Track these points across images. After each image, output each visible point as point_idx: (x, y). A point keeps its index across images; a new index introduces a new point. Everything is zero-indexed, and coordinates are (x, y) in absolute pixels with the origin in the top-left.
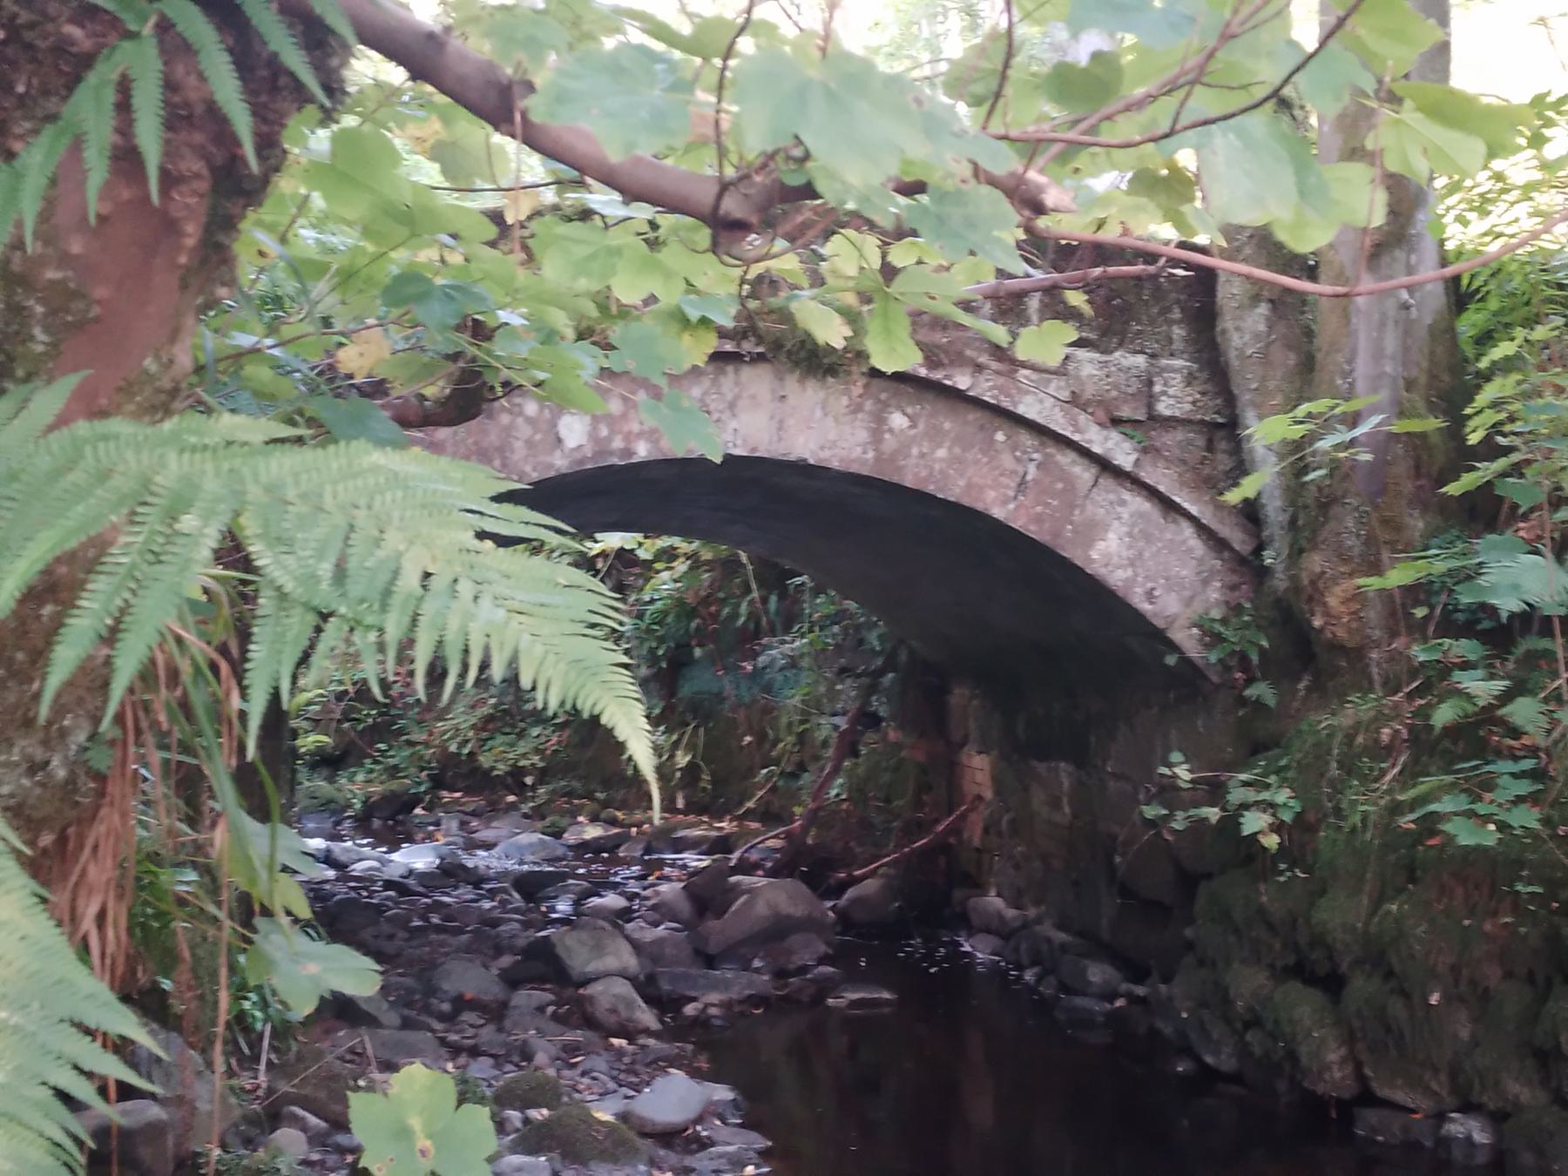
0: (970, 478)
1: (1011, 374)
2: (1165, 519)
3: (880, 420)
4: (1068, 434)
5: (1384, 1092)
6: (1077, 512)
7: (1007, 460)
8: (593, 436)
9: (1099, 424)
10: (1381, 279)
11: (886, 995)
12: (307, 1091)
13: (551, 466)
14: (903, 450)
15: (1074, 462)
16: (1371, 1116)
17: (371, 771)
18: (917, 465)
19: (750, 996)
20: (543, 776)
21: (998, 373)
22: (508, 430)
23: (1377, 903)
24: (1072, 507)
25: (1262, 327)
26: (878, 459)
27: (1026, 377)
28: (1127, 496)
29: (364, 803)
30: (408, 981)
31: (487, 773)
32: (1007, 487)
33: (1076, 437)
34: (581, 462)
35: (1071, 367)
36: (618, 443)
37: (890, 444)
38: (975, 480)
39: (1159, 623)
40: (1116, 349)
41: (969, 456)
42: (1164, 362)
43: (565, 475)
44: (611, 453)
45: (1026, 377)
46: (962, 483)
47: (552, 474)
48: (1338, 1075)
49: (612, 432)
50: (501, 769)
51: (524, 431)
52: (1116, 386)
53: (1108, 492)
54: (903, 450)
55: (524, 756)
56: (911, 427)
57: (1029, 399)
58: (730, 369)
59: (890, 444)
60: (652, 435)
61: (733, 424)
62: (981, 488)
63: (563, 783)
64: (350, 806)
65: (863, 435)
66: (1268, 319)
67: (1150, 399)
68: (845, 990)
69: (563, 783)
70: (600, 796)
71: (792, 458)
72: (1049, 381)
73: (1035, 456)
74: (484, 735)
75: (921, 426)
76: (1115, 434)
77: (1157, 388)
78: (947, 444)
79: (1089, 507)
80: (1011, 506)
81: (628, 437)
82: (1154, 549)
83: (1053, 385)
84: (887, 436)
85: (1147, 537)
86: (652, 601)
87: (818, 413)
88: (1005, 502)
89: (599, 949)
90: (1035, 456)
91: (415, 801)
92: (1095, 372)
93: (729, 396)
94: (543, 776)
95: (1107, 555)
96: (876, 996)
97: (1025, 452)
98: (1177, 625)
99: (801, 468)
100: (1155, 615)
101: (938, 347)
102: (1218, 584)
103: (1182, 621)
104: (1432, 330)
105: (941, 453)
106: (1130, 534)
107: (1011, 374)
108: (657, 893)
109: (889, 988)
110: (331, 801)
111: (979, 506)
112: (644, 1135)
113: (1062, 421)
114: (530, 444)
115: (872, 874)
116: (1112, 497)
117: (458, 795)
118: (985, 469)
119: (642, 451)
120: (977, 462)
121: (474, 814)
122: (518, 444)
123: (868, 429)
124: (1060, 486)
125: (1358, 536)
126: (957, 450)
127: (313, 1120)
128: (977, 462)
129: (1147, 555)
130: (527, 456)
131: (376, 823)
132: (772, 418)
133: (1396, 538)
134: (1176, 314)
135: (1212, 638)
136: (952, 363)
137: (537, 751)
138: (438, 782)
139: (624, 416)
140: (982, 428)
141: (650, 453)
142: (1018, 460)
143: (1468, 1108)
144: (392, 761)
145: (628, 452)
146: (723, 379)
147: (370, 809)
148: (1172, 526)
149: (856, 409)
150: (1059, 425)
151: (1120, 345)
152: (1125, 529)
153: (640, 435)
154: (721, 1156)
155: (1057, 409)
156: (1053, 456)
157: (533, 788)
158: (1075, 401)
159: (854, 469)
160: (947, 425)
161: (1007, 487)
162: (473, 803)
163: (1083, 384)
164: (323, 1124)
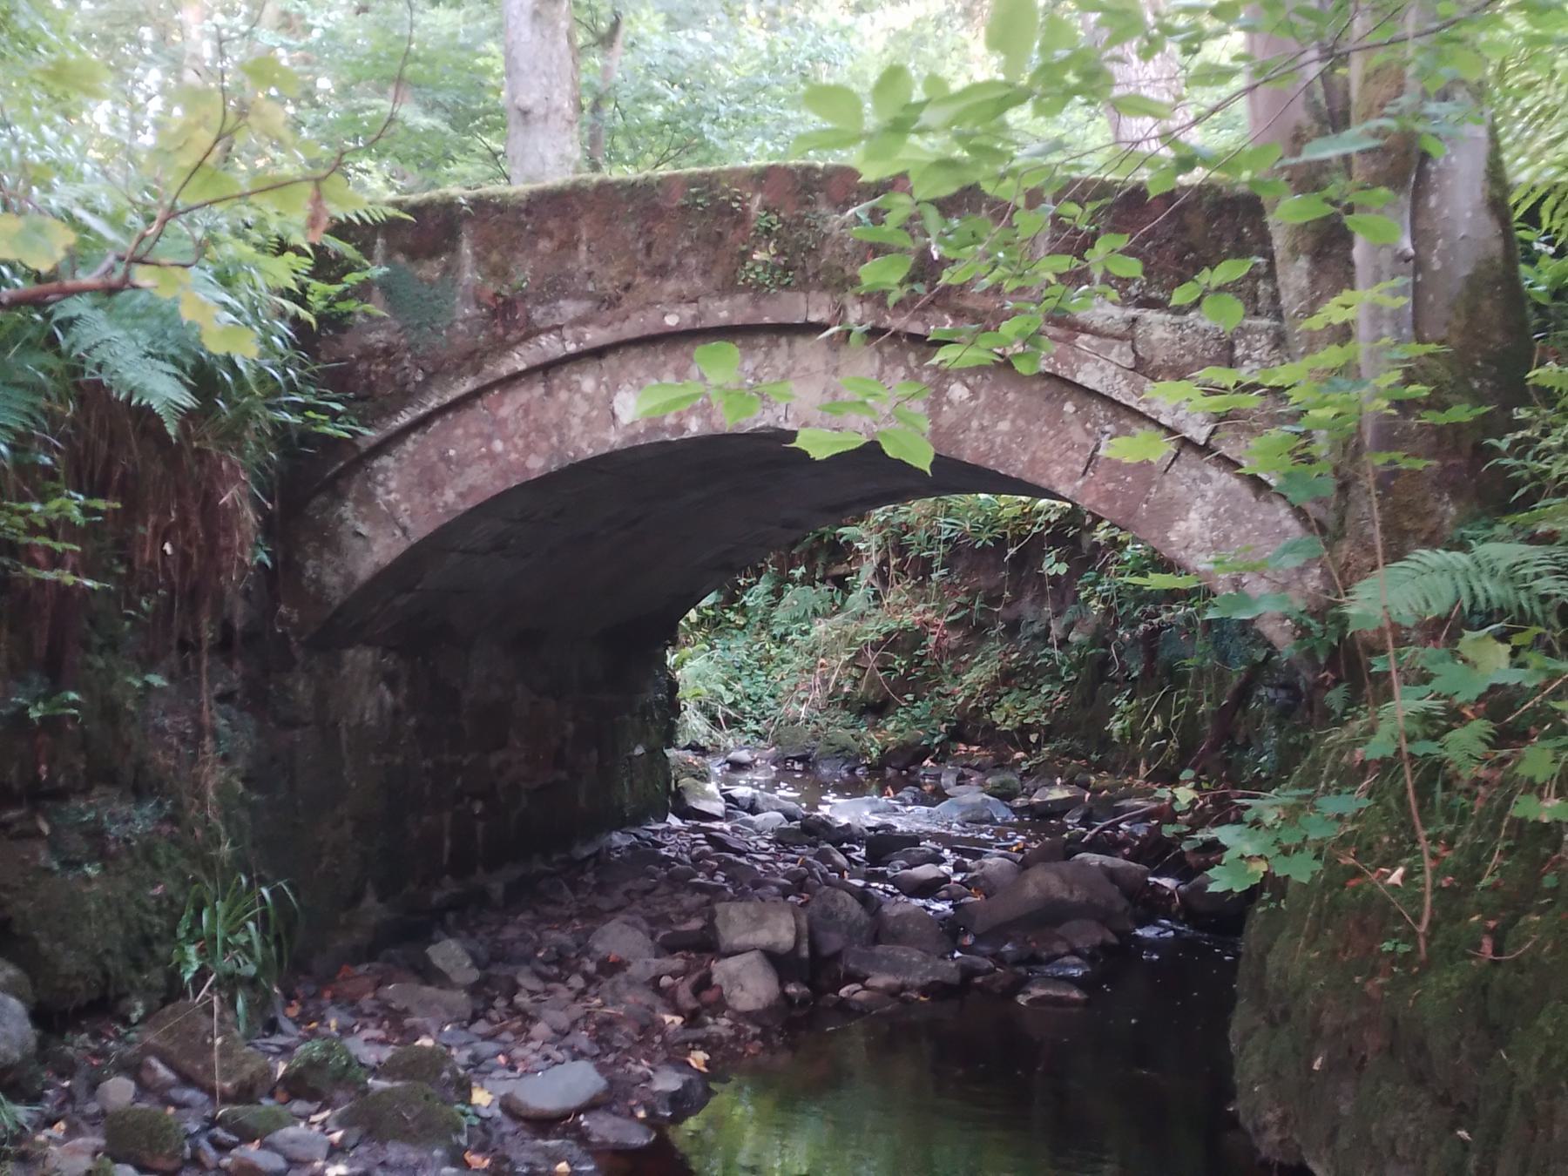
1: (1069, 340)
2: (1256, 496)
4: (1132, 404)
6: (1153, 490)
7: (1077, 434)
10: (96, 267)
12: (164, 1044)
13: (605, 442)
14: (963, 423)
18: (977, 438)
20: (1049, 734)
21: (1054, 339)
22: (565, 408)
24: (1148, 484)
25: (1305, 282)
28: (1213, 472)
29: (882, 752)
32: (1076, 462)
33: (1142, 408)
34: (635, 437)
37: (948, 415)
38: (1040, 454)
41: (1034, 429)
43: (616, 452)
44: (664, 430)
46: (1025, 458)
47: (607, 450)
51: (582, 407)
52: (1191, 350)
53: (1190, 467)
54: (963, 423)
56: (971, 399)
57: (1088, 367)
58: (783, 341)
59: (948, 415)
60: (705, 411)
62: (1047, 464)
63: (1066, 742)
64: (869, 754)
66: (1310, 274)
69: (1066, 742)
72: (1112, 347)
73: (1107, 428)
77: (1239, 352)
78: (1010, 416)
79: (1168, 485)
80: (1079, 483)
82: (1243, 530)
83: (1116, 350)
84: (945, 408)
85: (1236, 518)
88: (1072, 479)
89: (758, 922)
90: (1107, 428)
91: (926, 752)
92: (1166, 335)
93: (782, 370)
94: (1049, 734)
96: (1064, 994)
97: (1095, 424)
102: (1318, 571)
104: (1474, 284)
105: (1004, 426)
107: (1069, 340)
108: (982, 866)
113: (1125, 390)
114: (586, 420)
116: (1194, 472)
117: (975, 748)
118: (1051, 444)
119: (694, 427)
120: (1042, 435)
122: (576, 421)
126: (1021, 423)
128: (1042, 435)
129: (1233, 537)
130: (584, 432)
131: (890, 772)
132: (825, 391)
133: (1418, 526)
138: (956, 735)
140: (1048, 398)
141: (700, 427)
142: (1089, 433)
145: (681, 428)
146: (775, 352)
147: (886, 757)
148: (1265, 506)
152: (1210, 509)
155: (1120, 378)
157: (1038, 744)
160: (1011, 396)
161: (1076, 462)
163: (1153, 349)
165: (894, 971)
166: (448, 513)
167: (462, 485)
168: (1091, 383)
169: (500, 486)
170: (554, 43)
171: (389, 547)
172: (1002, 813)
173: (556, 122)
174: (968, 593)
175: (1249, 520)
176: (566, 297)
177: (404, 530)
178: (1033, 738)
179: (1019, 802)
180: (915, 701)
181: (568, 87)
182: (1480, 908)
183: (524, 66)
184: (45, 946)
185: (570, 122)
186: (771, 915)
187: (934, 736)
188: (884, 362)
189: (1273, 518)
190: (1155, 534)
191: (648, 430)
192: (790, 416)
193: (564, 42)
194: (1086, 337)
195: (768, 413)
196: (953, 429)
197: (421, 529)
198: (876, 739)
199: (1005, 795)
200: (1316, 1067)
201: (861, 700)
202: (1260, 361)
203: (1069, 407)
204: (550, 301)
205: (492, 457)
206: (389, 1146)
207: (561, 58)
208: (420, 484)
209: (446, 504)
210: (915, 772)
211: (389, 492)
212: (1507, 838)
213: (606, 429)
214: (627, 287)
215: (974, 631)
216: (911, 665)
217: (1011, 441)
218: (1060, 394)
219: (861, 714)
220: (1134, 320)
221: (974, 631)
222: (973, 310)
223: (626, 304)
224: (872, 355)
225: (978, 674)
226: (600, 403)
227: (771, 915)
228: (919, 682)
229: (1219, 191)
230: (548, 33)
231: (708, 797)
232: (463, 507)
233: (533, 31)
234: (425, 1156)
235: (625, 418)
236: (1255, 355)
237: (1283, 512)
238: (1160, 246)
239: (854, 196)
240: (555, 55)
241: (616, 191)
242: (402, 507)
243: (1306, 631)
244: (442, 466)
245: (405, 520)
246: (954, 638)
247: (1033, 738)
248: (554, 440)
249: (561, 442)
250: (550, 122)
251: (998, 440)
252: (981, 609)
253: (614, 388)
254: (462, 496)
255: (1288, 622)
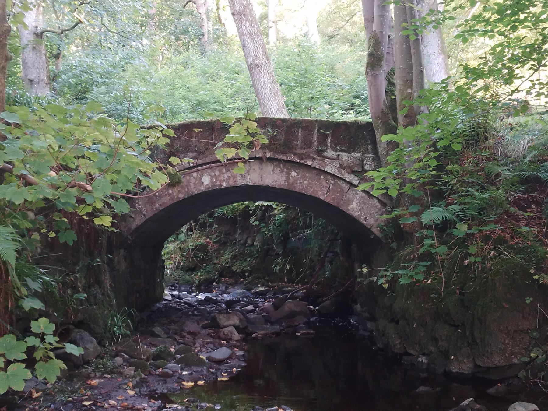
0: (314, 189)
1: (323, 160)
3: (289, 174)
4: (340, 176)
5: (409, 351)
6: (344, 197)
7: (324, 183)
8: (211, 181)
9: (348, 173)
11: (312, 332)
13: (201, 190)
14: (295, 181)
15: (343, 183)
16: (405, 357)
17: (202, 272)
18: (299, 186)
19: (273, 332)
20: (251, 273)
21: (319, 160)
22: (189, 181)
23: (406, 301)
26: (288, 184)
27: (328, 161)
29: (199, 282)
30: (177, 328)
31: (234, 272)
33: (342, 177)
34: (208, 188)
35: (340, 158)
36: (218, 183)
39: (369, 227)
40: (353, 152)
42: (366, 155)
44: (216, 186)
45: (328, 161)
46: (312, 190)
48: (399, 347)
49: (216, 180)
50: (238, 271)
51: (193, 181)
52: (353, 162)
55: (245, 267)
56: (297, 176)
57: (328, 167)
61: (249, 177)
62: (317, 191)
65: (284, 178)
67: (363, 166)
68: (301, 330)
69: (257, 275)
70: (267, 278)
71: (265, 185)
73: (332, 182)
74: (234, 261)
75: (300, 175)
76: (352, 176)
77: (364, 162)
79: (348, 195)
80: (326, 196)
81: (221, 181)
83: (335, 163)
84: (291, 178)
86: (278, 220)
87: (272, 173)
88: (324, 195)
89: (229, 319)
90: (332, 182)
94: (251, 273)
95: (353, 208)
98: (373, 227)
99: (268, 187)
100: (367, 224)
101: (302, 154)
103: (375, 226)
105: (306, 182)
106: (359, 202)
107: (323, 160)
108: (263, 305)
109: (313, 330)
110: (189, 281)
111: (317, 196)
112: (213, 362)
114: (194, 184)
115: (328, 299)
117: (227, 279)
119: (225, 185)
121: (231, 284)
122: (192, 184)
123: (286, 177)
124: (339, 190)
125: (409, 203)
126: (310, 181)
127: (126, 356)
131: (202, 287)
134: (369, 142)
135: (382, 230)
136: (306, 158)
137: (249, 265)
138: (221, 275)
139: (219, 176)
140: (317, 175)
143: (424, 354)
144: (208, 269)
145: (221, 185)
147: (201, 283)
148: (371, 200)
149: (282, 171)
150: (337, 173)
151: (354, 151)
152: (358, 201)
153: (224, 180)
154: (227, 366)
155: (336, 169)
156: (337, 182)
158: (341, 166)
159: (282, 187)
160: (307, 175)
162: (230, 281)
164: (128, 357)
165: (263, 330)
166: (157, 210)
167: (160, 203)
168: (329, 171)
169: (171, 202)
170: (41, 58)
171: (140, 220)
172: (248, 294)
173: (42, 84)
174: (219, 232)
175: (368, 204)
176: (190, 152)
177: (144, 215)
178: (246, 274)
179: (253, 291)
180: (206, 266)
181: (46, 72)
182: (454, 285)
183: (29, 65)
184: (92, 326)
185: (47, 84)
186: (231, 317)
187: (215, 276)
188: (274, 167)
189: (374, 203)
190: (345, 208)
191: (212, 186)
192: (250, 181)
193: (44, 57)
194: (327, 160)
195: (244, 180)
196: (293, 183)
197: (149, 215)
198: (197, 277)
199: (249, 290)
200: (414, 326)
201: (187, 267)
202: (370, 165)
203: (322, 177)
204: (185, 153)
205: (169, 195)
206: (193, 367)
207: (43, 63)
208: (148, 203)
209: (156, 208)
210: (210, 287)
211: (140, 205)
212: (457, 269)
213: (201, 186)
214: (207, 149)
215: (222, 244)
216: (204, 255)
217: (308, 186)
218: (320, 174)
219: (187, 271)
220: (339, 155)
221: (222, 244)
222: (299, 154)
223: (207, 153)
224: (271, 165)
225: (227, 256)
226: (198, 179)
227: (231, 317)
228: (206, 260)
229: (358, 123)
230: (38, 54)
231: (166, 295)
232: (161, 208)
233: (33, 54)
234: (202, 369)
235: (205, 183)
236: (368, 163)
237: (376, 201)
238: (345, 137)
239: (267, 125)
240: (41, 62)
241: (203, 124)
242: (144, 209)
243: (384, 230)
244: (155, 197)
245: (144, 212)
246: (216, 246)
247: (246, 274)
248: (186, 189)
249: (188, 190)
250: (40, 84)
251: (305, 186)
252: (224, 237)
253: (202, 176)
254: (160, 205)
255: (378, 228)
